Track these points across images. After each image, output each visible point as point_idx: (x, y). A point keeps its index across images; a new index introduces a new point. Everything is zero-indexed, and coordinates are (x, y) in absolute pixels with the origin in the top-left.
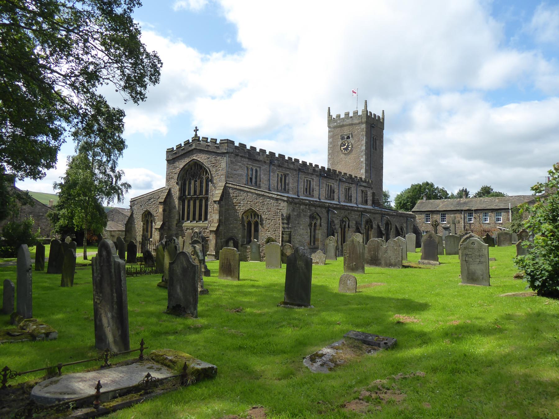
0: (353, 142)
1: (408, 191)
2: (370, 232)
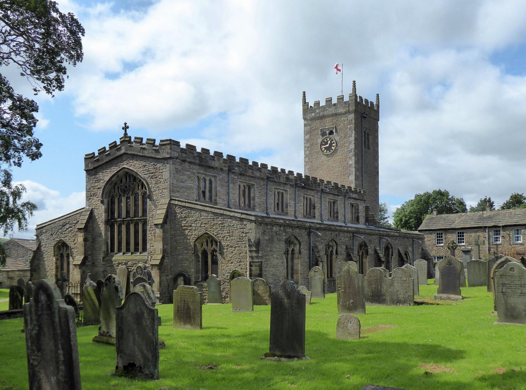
0: (337, 138)
1: (411, 203)
2: (364, 260)
